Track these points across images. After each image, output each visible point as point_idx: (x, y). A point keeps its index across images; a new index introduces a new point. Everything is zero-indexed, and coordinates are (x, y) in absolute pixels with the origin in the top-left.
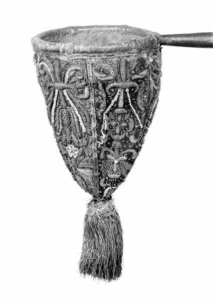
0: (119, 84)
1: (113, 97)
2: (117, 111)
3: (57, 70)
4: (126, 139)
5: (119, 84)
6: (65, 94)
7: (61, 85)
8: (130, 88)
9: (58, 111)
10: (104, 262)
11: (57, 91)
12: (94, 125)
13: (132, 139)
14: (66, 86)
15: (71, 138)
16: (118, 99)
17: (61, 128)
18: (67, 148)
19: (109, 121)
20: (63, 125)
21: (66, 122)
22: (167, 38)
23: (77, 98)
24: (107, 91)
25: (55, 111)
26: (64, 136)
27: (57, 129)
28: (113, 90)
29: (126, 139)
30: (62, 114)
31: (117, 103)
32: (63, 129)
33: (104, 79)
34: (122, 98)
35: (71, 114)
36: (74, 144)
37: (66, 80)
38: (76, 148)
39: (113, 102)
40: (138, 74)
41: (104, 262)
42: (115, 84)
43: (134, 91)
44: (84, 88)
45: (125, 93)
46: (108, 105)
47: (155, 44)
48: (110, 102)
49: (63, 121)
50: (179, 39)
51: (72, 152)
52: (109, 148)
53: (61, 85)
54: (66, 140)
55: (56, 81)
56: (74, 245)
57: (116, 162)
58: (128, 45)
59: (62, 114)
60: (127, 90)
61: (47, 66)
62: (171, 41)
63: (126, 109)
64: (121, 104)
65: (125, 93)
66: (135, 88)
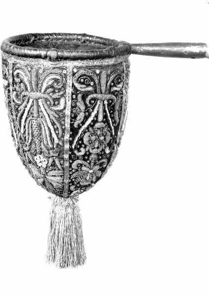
0: (99, 96)
1: (93, 109)
2: (97, 125)
3: (34, 79)
4: (103, 150)
5: (99, 96)
6: (40, 104)
7: (38, 94)
8: (108, 101)
9: (27, 122)
10: (69, 249)
11: (31, 101)
12: (67, 137)
13: (108, 151)
14: (43, 95)
15: (41, 149)
16: (98, 112)
17: (30, 138)
18: (35, 157)
19: (89, 136)
20: (33, 136)
21: (36, 133)
22: (138, 47)
23: (51, 110)
24: (88, 102)
25: (25, 121)
26: (33, 146)
27: (27, 139)
28: (93, 102)
29: (103, 150)
30: (32, 125)
31: (96, 116)
32: (32, 140)
33: (83, 90)
34: (101, 110)
35: (42, 126)
36: (44, 154)
37: (43, 91)
38: (44, 159)
39: (93, 114)
40: (116, 86)
41: (69, 249)
42: (95, 95)
43: (111, 103)
44: (59, 99)
45: (104, 105)
46: (86, 118)
47: (128, 50)
48: (90, 115)
49: (32, 133)
50: (150, 49)
51: (41, 162)
52: (86, 161)
53: (38, 94)
54: (36, 150)
55: (32, 90)
56: (40, 240)
57: (91, 171)
58: (109, 52)
59: (32, 125)
60: (106, 102)
61: (23, 73)
62: (142, 50)
63: (104, 122)
64: (100, 118)
65: (104, 105)
66: (112, 100)
